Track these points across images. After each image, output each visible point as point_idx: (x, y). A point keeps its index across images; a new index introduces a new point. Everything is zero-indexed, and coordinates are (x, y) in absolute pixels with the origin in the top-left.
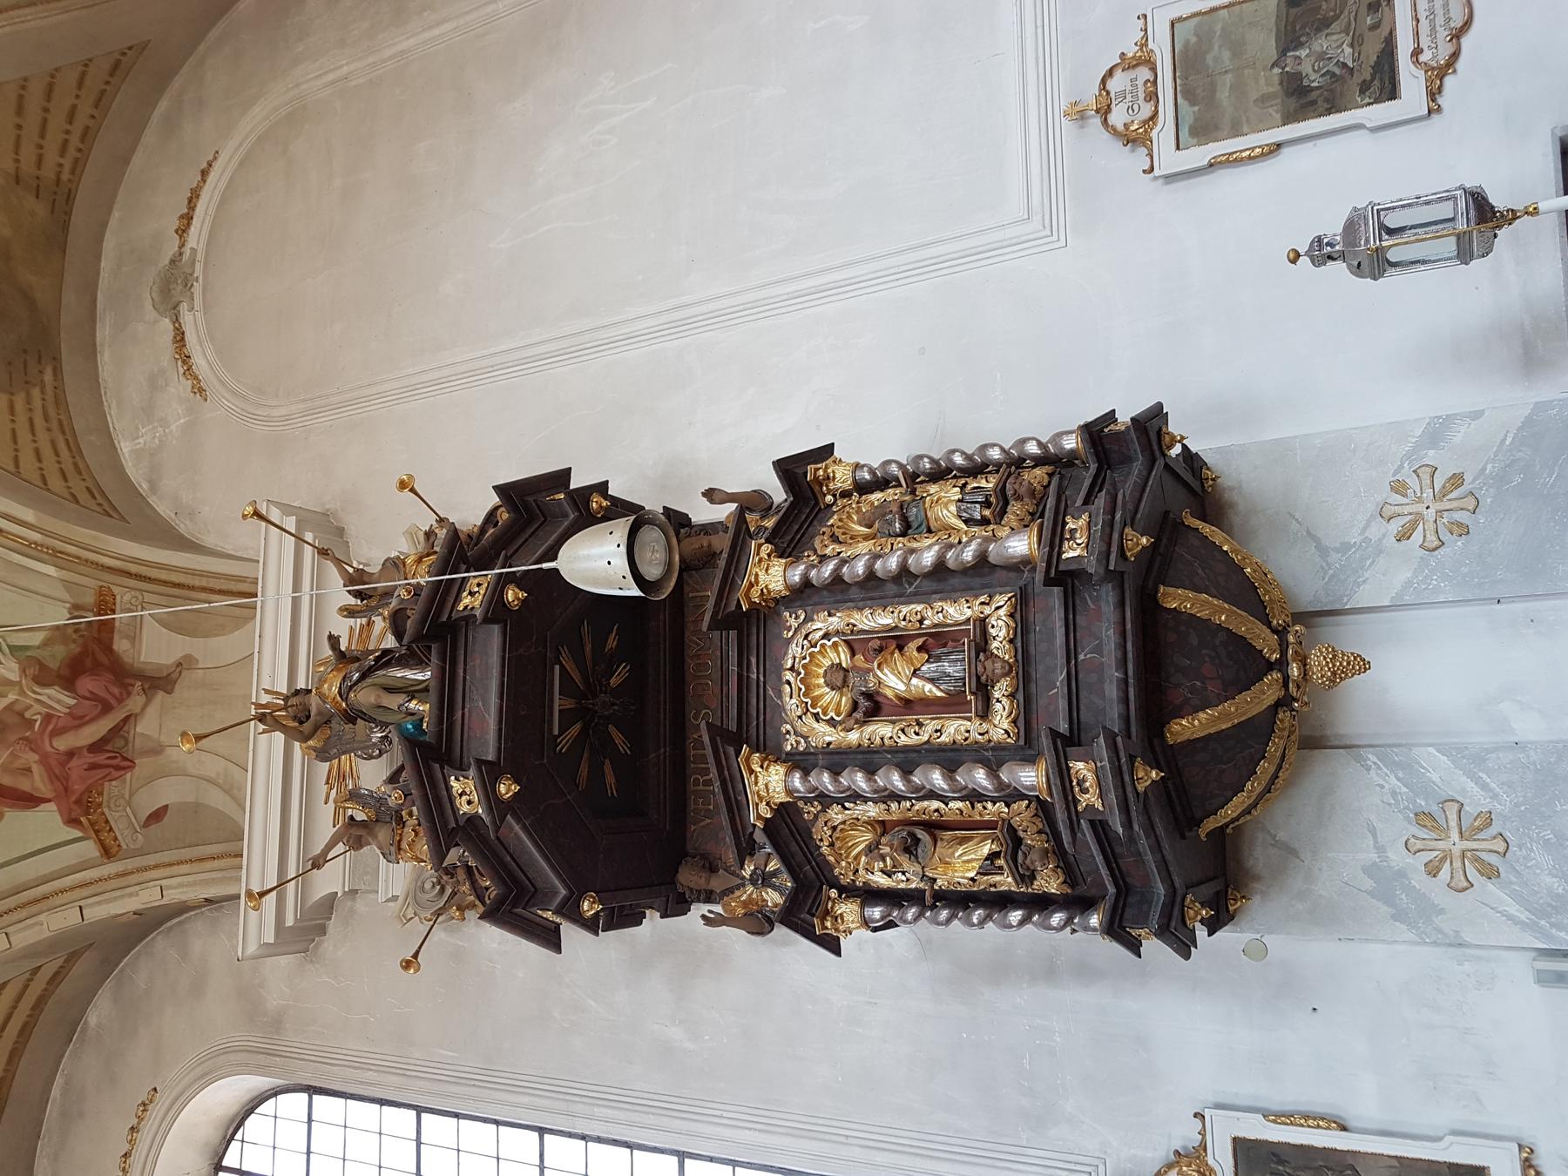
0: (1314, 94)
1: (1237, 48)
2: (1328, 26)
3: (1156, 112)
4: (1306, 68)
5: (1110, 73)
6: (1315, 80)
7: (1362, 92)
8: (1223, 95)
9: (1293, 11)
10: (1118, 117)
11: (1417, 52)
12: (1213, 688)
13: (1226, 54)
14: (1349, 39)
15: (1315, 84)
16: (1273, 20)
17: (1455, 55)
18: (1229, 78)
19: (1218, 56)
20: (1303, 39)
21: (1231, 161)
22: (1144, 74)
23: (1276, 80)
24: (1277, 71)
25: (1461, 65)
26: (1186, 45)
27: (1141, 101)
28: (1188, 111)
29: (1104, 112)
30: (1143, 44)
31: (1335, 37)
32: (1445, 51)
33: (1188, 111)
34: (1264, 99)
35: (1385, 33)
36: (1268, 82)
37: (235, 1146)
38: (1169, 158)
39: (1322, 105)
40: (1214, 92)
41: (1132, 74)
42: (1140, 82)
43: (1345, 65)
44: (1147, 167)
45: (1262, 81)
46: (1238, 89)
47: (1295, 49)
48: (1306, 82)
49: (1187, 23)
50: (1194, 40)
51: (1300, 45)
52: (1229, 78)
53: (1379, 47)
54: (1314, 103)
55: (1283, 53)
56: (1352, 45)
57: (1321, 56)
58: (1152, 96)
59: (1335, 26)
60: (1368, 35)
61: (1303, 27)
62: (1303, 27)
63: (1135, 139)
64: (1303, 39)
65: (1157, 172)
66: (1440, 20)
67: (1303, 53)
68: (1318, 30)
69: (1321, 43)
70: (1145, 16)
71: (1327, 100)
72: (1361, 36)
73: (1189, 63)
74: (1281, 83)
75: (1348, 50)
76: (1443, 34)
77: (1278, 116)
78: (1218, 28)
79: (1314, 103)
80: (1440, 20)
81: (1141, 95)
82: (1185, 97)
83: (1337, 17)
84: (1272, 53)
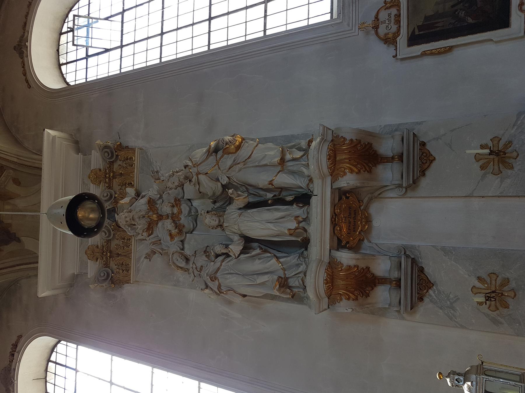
10: (382, 30)
21: (424, 54)
22: (394, 11)
29: (376, 28)
37: (54, 354)
38: (403, 48)
41: (389, 11)
58: (398, 22)
63: (390, 40)
65: (398, 57)
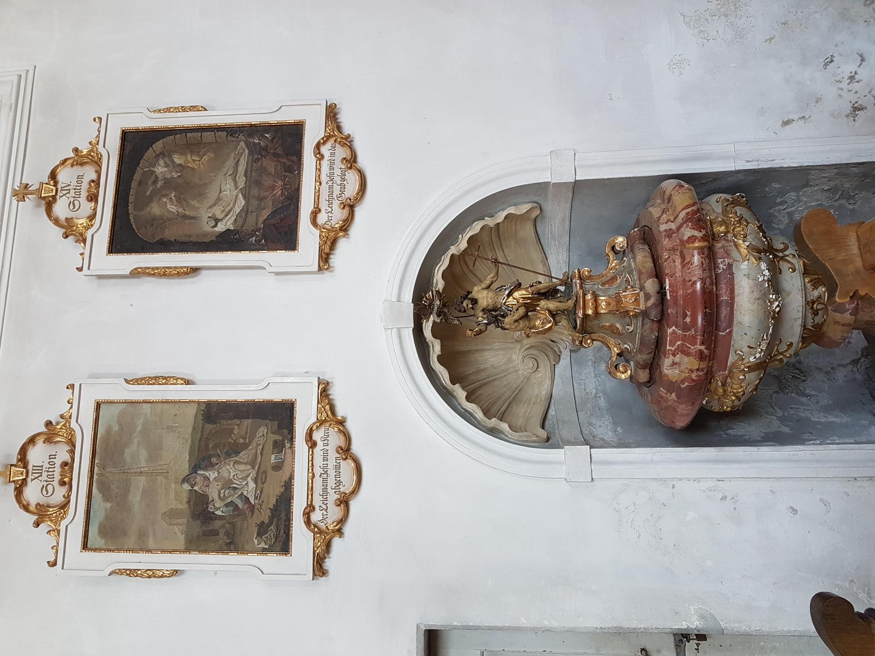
0: (217, 524)
1: (155, 450)
2: (237, 453)
3: (68, 498)
4: (213, 492)
5: (32, 440)
6: (219, 508)
7: (260, 534)
8: (135, 498)
9: (209, 427)
11: (310, 509)
12: (278, 549)
13: (143, 454)
14: (253, 474)
15: (218, 513)
16: (190, 431)
17: (343, 521)
18: (142, 481)
19: (137, 454)
20: (214, 460)
22: (89, 173)
23: (185, 497)
24: (187, 487)
25: (347, 529)
26: (109, 430)
27: (56, 483)
28: (100, 506)
30: (93, 145)
31: (242, 467)
32: (335, 513)
33: (100, 506)
34: (171, 514)
35: (285, 478)
36: (175, 497)
39: (223, 538)
40: (127, 491)
41: (78, 170)
42: (58, 462)
43: (247, 499)
44: (52, 559)
45: (172, 496)
46: (148, 494)
47: (206, 469)
48: (211, 508)
49: (112, 406)
50: (116, 428)
51: (210, 466)
52: (142, 481)
53: (279, 490)
54: (215, 533)
55: (195, 469)
56: (256, 481)
57: (228, 484)
59: (244, 456)
60: (270, 473)
61: (216, 446)
62: (216, 446)
64: (214, 460)
66: (331, 482)
67: (212, 475)
68: (228, 455)
69: (230, 470)
70: (100, 119)
71: (227, 534)
72: (265, 472)
73: (108, 451)
74: (188, 502)
75: (252, 485)
76: (333, 497)
77: (182, 538)
78: (140, 422)
79: (215, 533)
80: (331, 482)
81: (84, 194)
82: (100, 490)
83: (245, 446)
84: (185, 467)
